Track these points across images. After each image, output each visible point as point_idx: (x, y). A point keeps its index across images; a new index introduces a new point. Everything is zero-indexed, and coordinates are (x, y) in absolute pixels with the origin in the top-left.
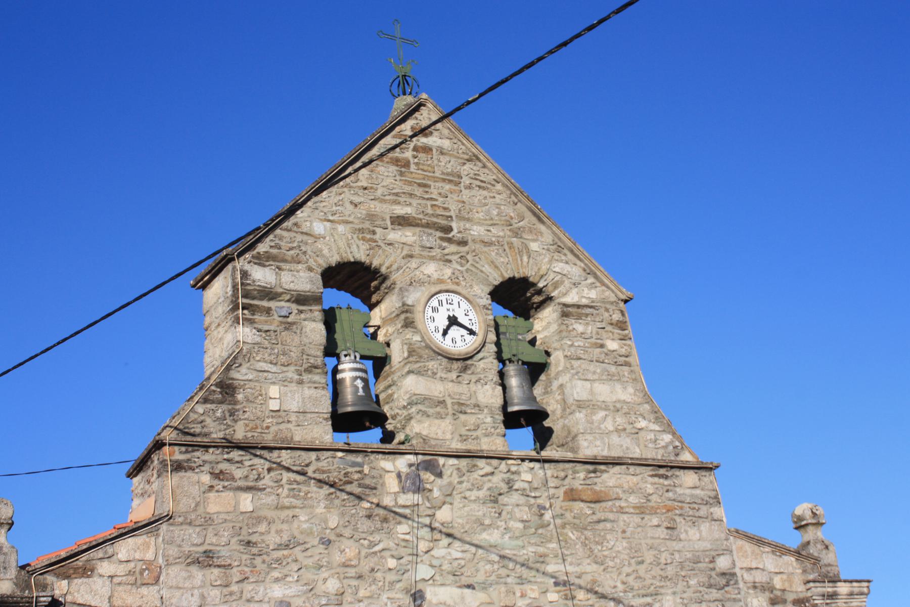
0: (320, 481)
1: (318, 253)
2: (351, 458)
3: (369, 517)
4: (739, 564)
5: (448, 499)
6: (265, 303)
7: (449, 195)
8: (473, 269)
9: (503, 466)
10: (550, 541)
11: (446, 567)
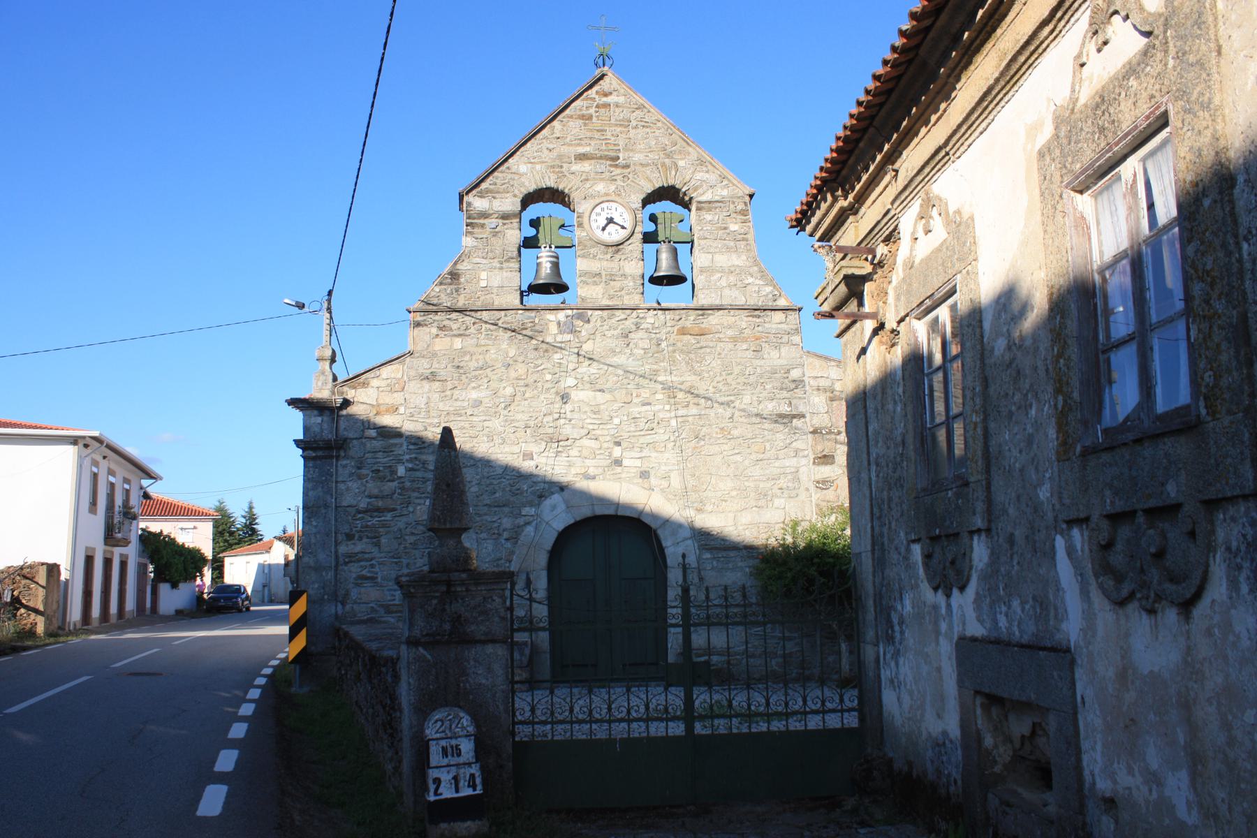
0: (505, 329)
1: (522, 185)
2: (528, 313)
3: (536, 349)
4: (807, 374)
5: (592, 336)
6: (482, 221)
7: (620, 135)
8: (633, 184)
9: (635, 313)
10: (663, 361)
11: (586, 378)
